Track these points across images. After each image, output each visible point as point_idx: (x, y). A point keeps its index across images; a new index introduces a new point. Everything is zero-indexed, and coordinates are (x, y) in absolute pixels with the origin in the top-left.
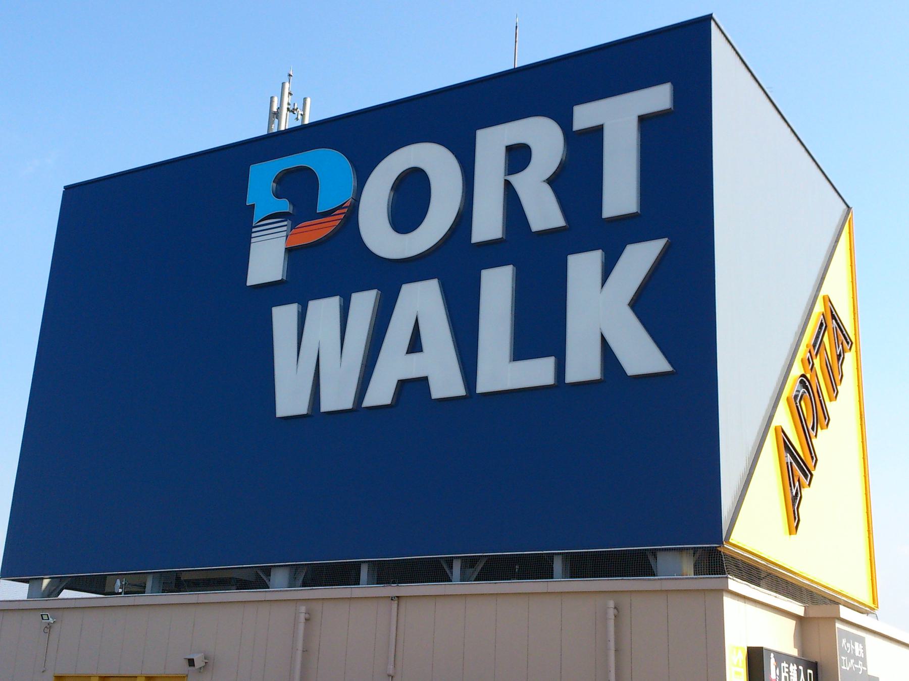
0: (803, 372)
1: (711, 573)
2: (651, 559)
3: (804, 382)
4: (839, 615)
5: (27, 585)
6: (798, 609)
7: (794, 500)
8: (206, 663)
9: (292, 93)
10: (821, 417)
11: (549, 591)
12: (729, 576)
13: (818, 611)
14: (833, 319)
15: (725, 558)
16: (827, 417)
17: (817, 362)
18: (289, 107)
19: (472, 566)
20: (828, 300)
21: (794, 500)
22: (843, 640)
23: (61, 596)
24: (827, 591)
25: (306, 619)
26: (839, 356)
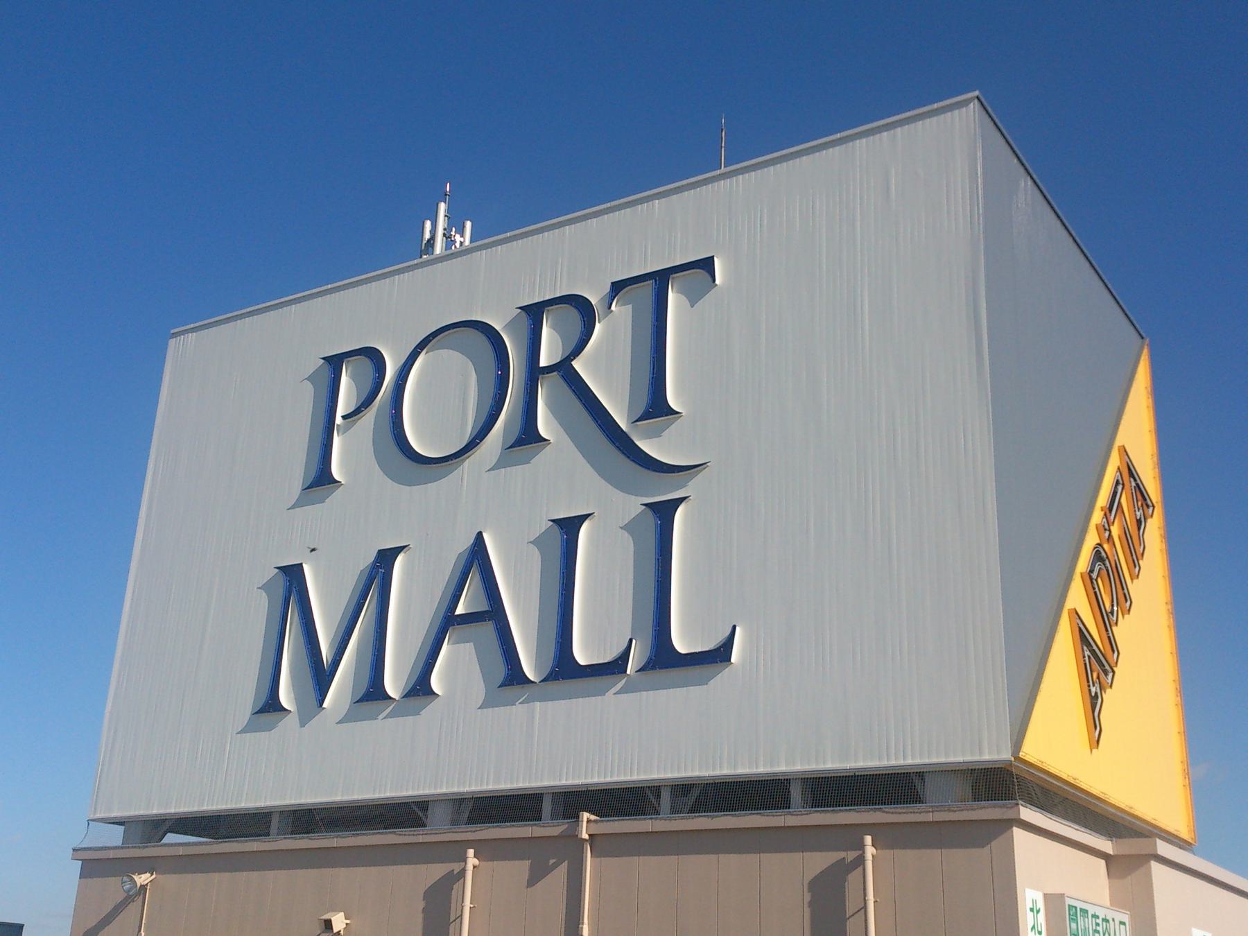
0: (1098, 541)
1: (997, 798)
2: (917, 782)
3: (1098, 556)
4: (1157, 850)
5: (123, 827)
6: (1106, 846)
7: (1093, 703)
8: (347, 924)
9: (313, 547)
10: (1123, 599)
11: (935, 820)
12: (1020, 802)
13: (1130, 846)
14: (1130, 476)
15: (1017, 779)
16: (1127, 597)
17: (1115, 530)
18: (446, 232)
19: (684, 795)
20: (1124, 451)
21: (1093, 703)
22: (550, 864)
23: (165, 840)
24: (1069, 824)
25: (74, 850)
26: (1139, 522)
